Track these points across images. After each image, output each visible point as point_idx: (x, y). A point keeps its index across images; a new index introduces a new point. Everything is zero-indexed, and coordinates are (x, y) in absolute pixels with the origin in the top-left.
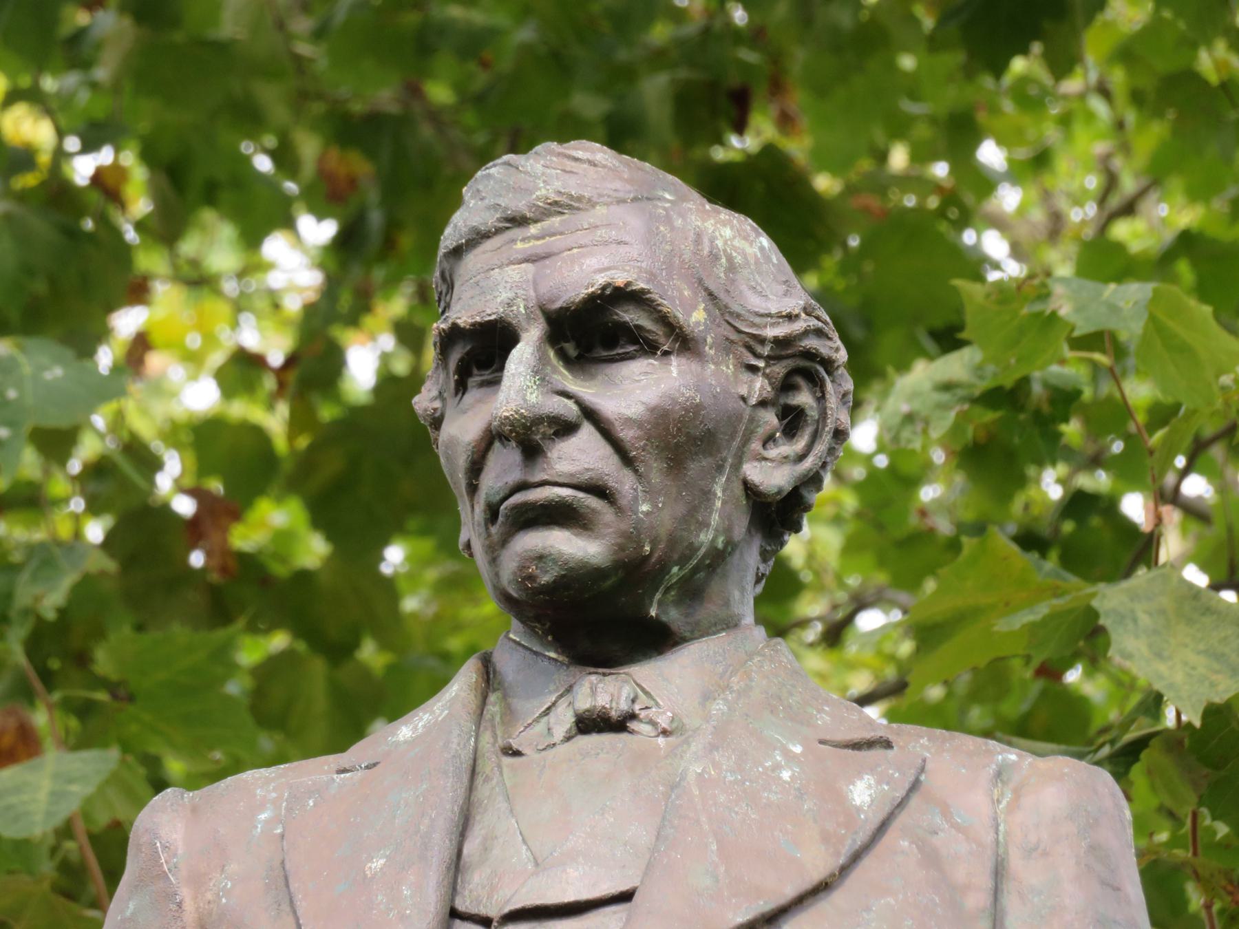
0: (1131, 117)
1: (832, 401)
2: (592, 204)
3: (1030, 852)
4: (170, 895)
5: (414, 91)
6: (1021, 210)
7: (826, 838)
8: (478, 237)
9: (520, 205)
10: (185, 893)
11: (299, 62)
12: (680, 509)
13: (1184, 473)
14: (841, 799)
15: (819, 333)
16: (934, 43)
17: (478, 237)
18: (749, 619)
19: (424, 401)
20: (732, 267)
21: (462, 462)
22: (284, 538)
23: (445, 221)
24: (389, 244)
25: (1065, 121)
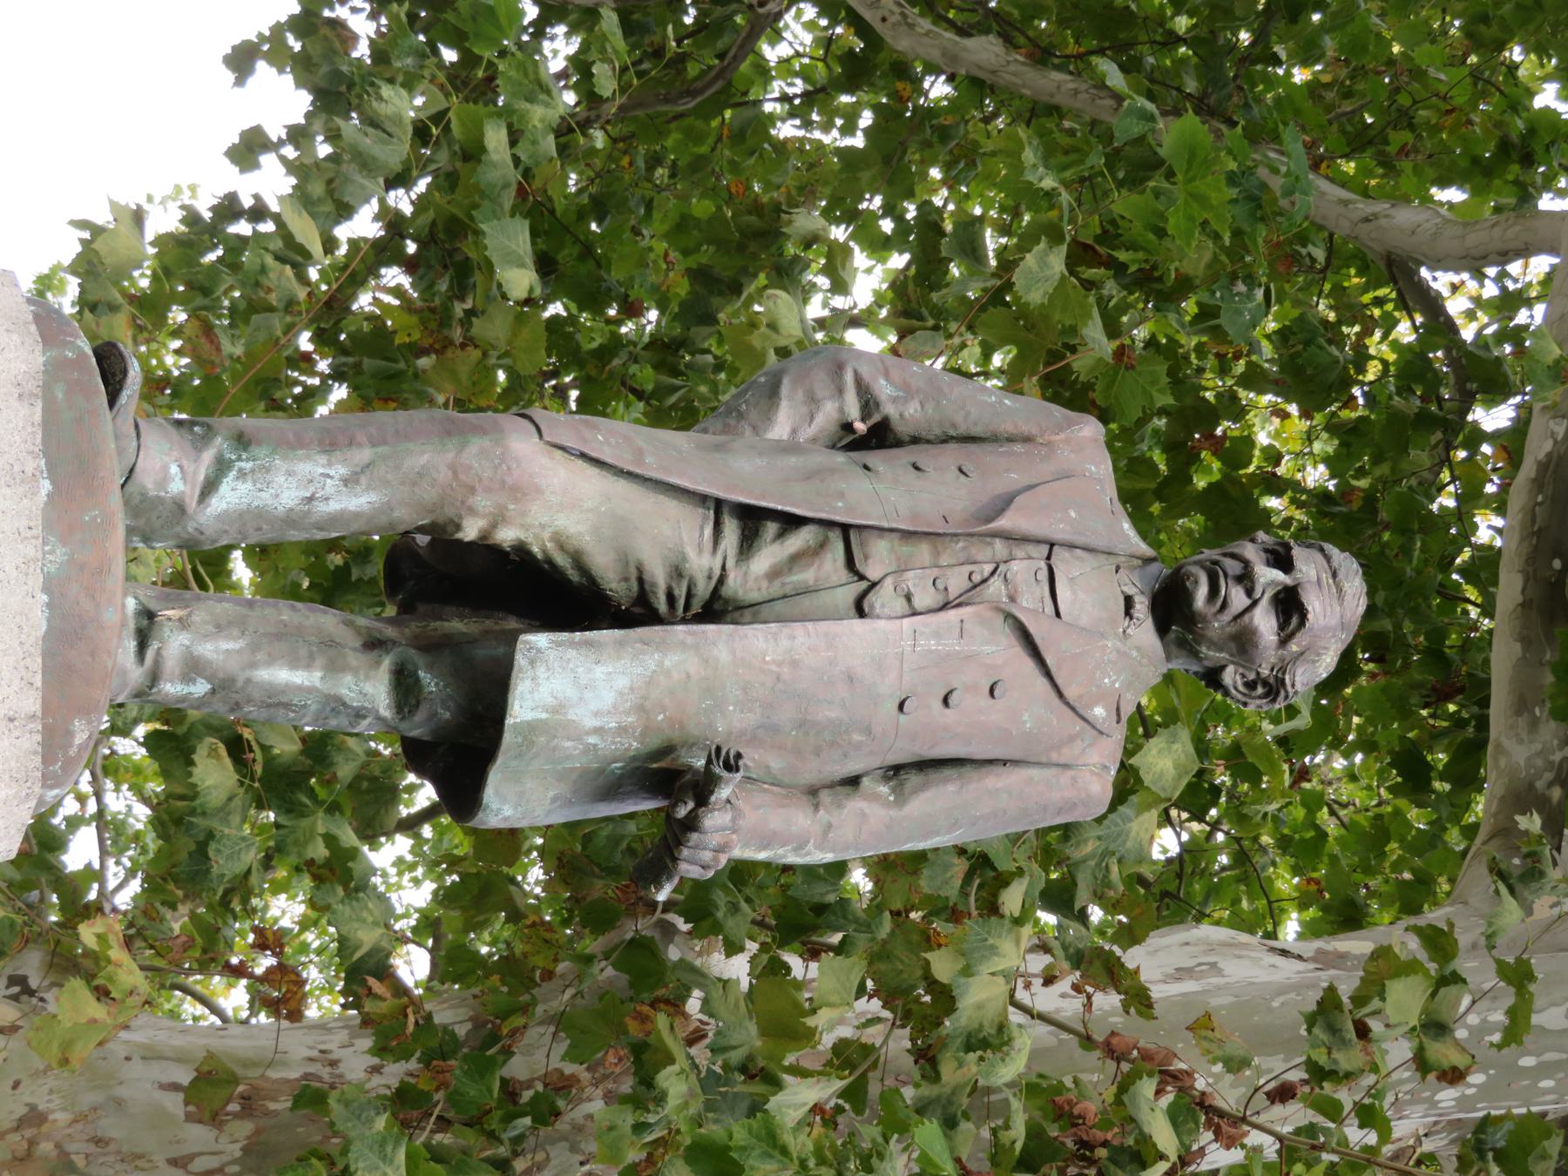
0: (1370, 814)
1: (1258, 702)
2: (1341, 605)
3: (1074, 780)
4: (1061, 429)
5: (1387, 527)
6: (1333, 769)
7: (1080, 697)
8: (1328, 558)
9: (1341, 575)
10: (1062, 436)
11: (1398, 482)
12: (1216, 639)
13: (1227, 833)
14: (1096, 703)
15: (1286, 697)
16: (1403, 738)
17: (1328, 558)
18: (1170, 666)
19: (1261, 536)
20: (1314, 662)
21: (1236, 551)
22: (1209, 470)
23: (1335, 545)
24: (1324, 514)
25: (1369, 788)
